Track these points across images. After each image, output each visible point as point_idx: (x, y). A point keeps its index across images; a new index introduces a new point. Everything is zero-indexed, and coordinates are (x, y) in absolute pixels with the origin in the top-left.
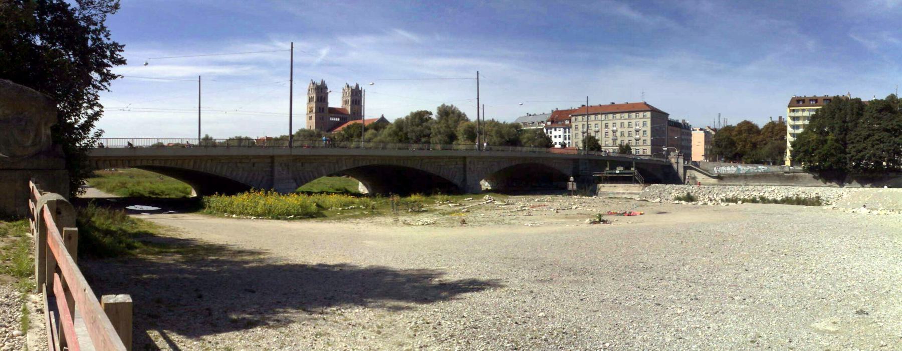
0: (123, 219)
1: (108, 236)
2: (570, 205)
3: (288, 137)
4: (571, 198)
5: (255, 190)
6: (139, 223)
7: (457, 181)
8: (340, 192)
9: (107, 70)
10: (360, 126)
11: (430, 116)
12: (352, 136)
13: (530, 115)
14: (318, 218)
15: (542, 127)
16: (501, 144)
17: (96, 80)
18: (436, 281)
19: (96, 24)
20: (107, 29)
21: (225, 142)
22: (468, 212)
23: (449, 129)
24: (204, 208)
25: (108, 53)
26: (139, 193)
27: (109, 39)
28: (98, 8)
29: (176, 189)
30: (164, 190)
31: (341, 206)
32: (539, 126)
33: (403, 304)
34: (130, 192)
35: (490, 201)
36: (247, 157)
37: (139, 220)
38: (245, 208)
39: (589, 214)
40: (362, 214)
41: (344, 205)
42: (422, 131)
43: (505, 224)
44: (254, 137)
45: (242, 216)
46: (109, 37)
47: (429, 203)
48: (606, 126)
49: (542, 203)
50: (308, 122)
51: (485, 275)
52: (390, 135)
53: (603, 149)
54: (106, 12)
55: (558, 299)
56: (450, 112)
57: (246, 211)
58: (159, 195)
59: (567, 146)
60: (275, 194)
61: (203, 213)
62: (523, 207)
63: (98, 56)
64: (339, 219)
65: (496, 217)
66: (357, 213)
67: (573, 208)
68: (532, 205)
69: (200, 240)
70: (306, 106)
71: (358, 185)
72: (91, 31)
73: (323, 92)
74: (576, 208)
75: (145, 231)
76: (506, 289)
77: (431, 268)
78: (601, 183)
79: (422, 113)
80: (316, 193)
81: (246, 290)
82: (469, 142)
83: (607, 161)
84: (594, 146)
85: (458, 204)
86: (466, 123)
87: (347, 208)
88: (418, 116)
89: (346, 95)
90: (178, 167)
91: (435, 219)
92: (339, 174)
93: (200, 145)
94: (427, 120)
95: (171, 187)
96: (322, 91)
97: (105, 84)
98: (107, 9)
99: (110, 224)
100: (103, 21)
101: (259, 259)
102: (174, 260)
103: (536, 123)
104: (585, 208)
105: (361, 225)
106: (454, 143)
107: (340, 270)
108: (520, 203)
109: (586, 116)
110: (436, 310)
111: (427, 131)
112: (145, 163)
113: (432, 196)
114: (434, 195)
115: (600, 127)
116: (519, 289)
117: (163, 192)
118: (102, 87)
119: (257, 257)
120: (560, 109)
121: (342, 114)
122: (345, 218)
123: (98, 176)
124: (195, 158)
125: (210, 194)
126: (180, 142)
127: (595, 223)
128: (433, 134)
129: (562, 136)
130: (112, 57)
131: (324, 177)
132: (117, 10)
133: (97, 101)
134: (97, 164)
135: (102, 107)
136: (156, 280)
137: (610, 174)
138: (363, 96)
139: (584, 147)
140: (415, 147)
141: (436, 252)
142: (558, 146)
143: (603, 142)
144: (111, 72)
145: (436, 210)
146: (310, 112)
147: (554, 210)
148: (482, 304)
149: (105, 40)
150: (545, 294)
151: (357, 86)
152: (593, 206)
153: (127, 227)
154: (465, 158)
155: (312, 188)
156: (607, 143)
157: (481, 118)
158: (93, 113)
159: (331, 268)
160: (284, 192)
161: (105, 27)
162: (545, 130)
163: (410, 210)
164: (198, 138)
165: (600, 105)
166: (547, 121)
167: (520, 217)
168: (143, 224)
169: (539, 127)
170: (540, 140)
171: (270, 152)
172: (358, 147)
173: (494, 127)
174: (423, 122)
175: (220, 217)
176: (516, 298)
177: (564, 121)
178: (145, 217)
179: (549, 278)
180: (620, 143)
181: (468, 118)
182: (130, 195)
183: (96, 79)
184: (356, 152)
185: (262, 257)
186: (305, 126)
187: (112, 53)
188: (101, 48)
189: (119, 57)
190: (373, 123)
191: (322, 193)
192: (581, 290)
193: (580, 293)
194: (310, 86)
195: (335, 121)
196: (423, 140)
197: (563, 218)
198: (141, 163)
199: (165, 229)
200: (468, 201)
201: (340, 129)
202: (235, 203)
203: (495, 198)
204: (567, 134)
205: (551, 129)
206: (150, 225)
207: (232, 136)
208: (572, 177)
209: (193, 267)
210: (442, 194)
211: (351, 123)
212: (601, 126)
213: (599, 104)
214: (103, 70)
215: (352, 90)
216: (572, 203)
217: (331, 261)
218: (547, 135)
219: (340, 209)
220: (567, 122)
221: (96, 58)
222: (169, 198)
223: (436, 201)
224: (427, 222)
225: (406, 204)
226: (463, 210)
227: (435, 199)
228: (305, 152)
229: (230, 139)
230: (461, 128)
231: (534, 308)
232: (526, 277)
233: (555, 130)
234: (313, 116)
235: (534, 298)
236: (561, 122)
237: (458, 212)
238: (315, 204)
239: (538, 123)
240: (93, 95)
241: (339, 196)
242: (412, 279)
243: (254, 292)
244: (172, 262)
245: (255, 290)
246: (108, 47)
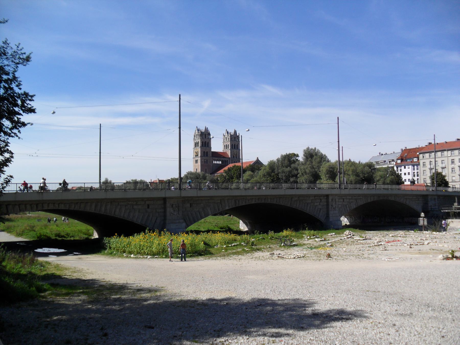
0: (32, 262)
1: (19, 281)
2: (422, 241)
3: (177, 179)
4: (422, 233)
5: (150, 230)
6: (47, 266)
7: (321, 216)
8: (224, 230)
9: (17, 118)
10: (239, 168)
11: (297, 158)
12: (232, 178)
13: (382, 155)
14: (206, 256)
15: (392, 166)
16: (356, 183)
17: (7, 127)
18: (309, 311)
19: (7, 74)
20: (19, 80)
21: (122, 185)
22: (332, 246)
23: (313, 170)
24: (105, 249)
25: (19, 102)
26: (46, 236)
27: (20, 89)
28: (11, 59)
29: (80, 231)
30: (69, 232)
31: (225, 244)
32: (390, 164)
33: (282, 331)
34: (38, 235)
35: (350, 236)
36: (142, 199)
37: (47, 262)
38: (141, 248)
39: (441, 250)
40: (244, 250)
41: (228, 243)
42: (290, 172)
43: (365, 258)
44: (148, 181)
45: (139, 256)
46: (20, 87)
47: (298, 237)
48: (453, 162)
49: (396, 238)
50: (194, 166)
51: (351, 306)
52: (264, 176)
53: (450, 185)
54: (18, 63)
55: (419, 333)
56: (314, 154)
57: (142, 251)
58: (65, 237)
59: (416, 183)
60: (168, 234)
61: (104, 254)
62: (379, 242)
63: (10, 104)
64: (224, 256)
65: (356, 252)
66: (239, 250)
67: (425, 243)
68: (387, 240)
69: (103, 280)
70: (193, 150)
71: (239, 222)
72: (3, 80)
73: (207, 137)
74: (428, 243)
75: (53, 274)
76: (371, 321)
77: (304, 299)
78: (449, 219)
79: (291, 155)
80: (203, 232)
81: (145, 326)
82: (331, 182)
83: (455, 196)
84: (441, 182)
85: (323, 239)
86: (327, 164)
87: (230, 245)
88: (287, 159)
89: (226, 140)
90: (80, 210)
91: (305, 252)
92: (222, 214)
93: (101, 188)
94: (294, 162)
95: (76, 229)
96: (205, 137)
97: (15, 131)
98: (19, 61)
99: (20, 268)
100: (15, 71)
101: (156, 296)
102: (80, 300)
103: (387, 161)
104: (436, 244)
105: (242, 261)
106: (317, 182)
107: (227, 304)
108: (376, 238)
109: (433, 154)
110: (312, 338)
111: (296, 172)
112: (51, 207)
113: (301, 232)
114: (303, 230)
116: (383, 322)
117: (68, 234)
118: (13, 135)
119: (153, 294)
121: (224, 157)
122: (228, 255)
123: (8, 220)
124: (99, 201)
125: (110, 235)
126: (83, 185)
127: (449, 259)
128: (300, 174)
129: (411, 173)
130: (23, 106)
131: (210, 216)
132: (28, 63)
133: (8, 147)
134: (7, 209)
135: (12, 154)
136: (65, 321)
137: (458, 209)
138: (240, 141)
139: (433, 183)
140: (284, 185)
141: (307, 284)
142: (407, 183)
143: (450, 178)
144: (21, 120)
145: (304, 244)
146: (196, 156)
147: (408, 245)
148: (351, 334)
149: (16, 90)
150: (407, 328)
151: (235, 132)
152: (445, 242)
153: (36, 270)
154: (327, 196)
155: (199, 227)
156: (454, 178)
157: (341, 160)
158: (3, 159)
159: (219, 302)
160: (175, 232)
161: (17, 78)
162: (395, 168)
163: (282, 244)
164: (99, 182)
165: (446, 142)
166: (397, 159)
167: (377, 251)
168: (51, 267)
169: (390, 166)
170: (391, 177)
171: (161, 194)
172: (238, 188)
173: (351, 166)
174: (292, 164)
175: (119, 257)
176: (381, 330)
177: (413, 159)
178: (52, 259)
179: (409, 312)
180: (410, 182)
181: (328, 159)
182: (38, 237)
183: (7, 126)
184: (237, 193)
185: (158, 294)
186: (192, 170)
187: (23, 102)
188: (13, 97)
189: (29, 106)
190: (250, 166)
191: (208, 231)
192: (441, 327)
193: (441, 330)
194: (195, 133)
195: (218, 164)
196: (292, 180)
197: (416, 254)
198: (48, 207)
199: (71, 270)
200: (332, 236)
201: (222, 171)
202: (133, 243)
203: (354, 233)
204: (416, 171)
205: (401, 166)
206: (57, 267)
207: (129, 179)
208: (423, 213)
209: (99, 307)
210: (309, 229)
211: (231, 165)
212: (447, 162)
213: (445, 141)
214: (14, 118)
215: (231, 136)
216: (424, 239)
217: (219, 296)
218: (397, 173)
219: (225, 246)
220: (415, 160)
221: (8, 106)
222: (74, 240)
223: (304, 235)
224: (298, 256)
225: (280, 239)
226: (328, 245)
227: (303, 234)
228: (193, 193)
229: (127, 183)
230: (324, 169)
231: (398, 341)
232: (388, 311)
233: (405, 168)
234: (199, 159)
235: (397, 331)
236: (410, 159)
237: (324, 246)
238: (203, 242)
239: (389, 162)
240: (4, 141)
241: (223, 234)
242: (289, 309)
243: (153, 328)
244: (79, 302)
245: (154, 325)
246: (19, 96)
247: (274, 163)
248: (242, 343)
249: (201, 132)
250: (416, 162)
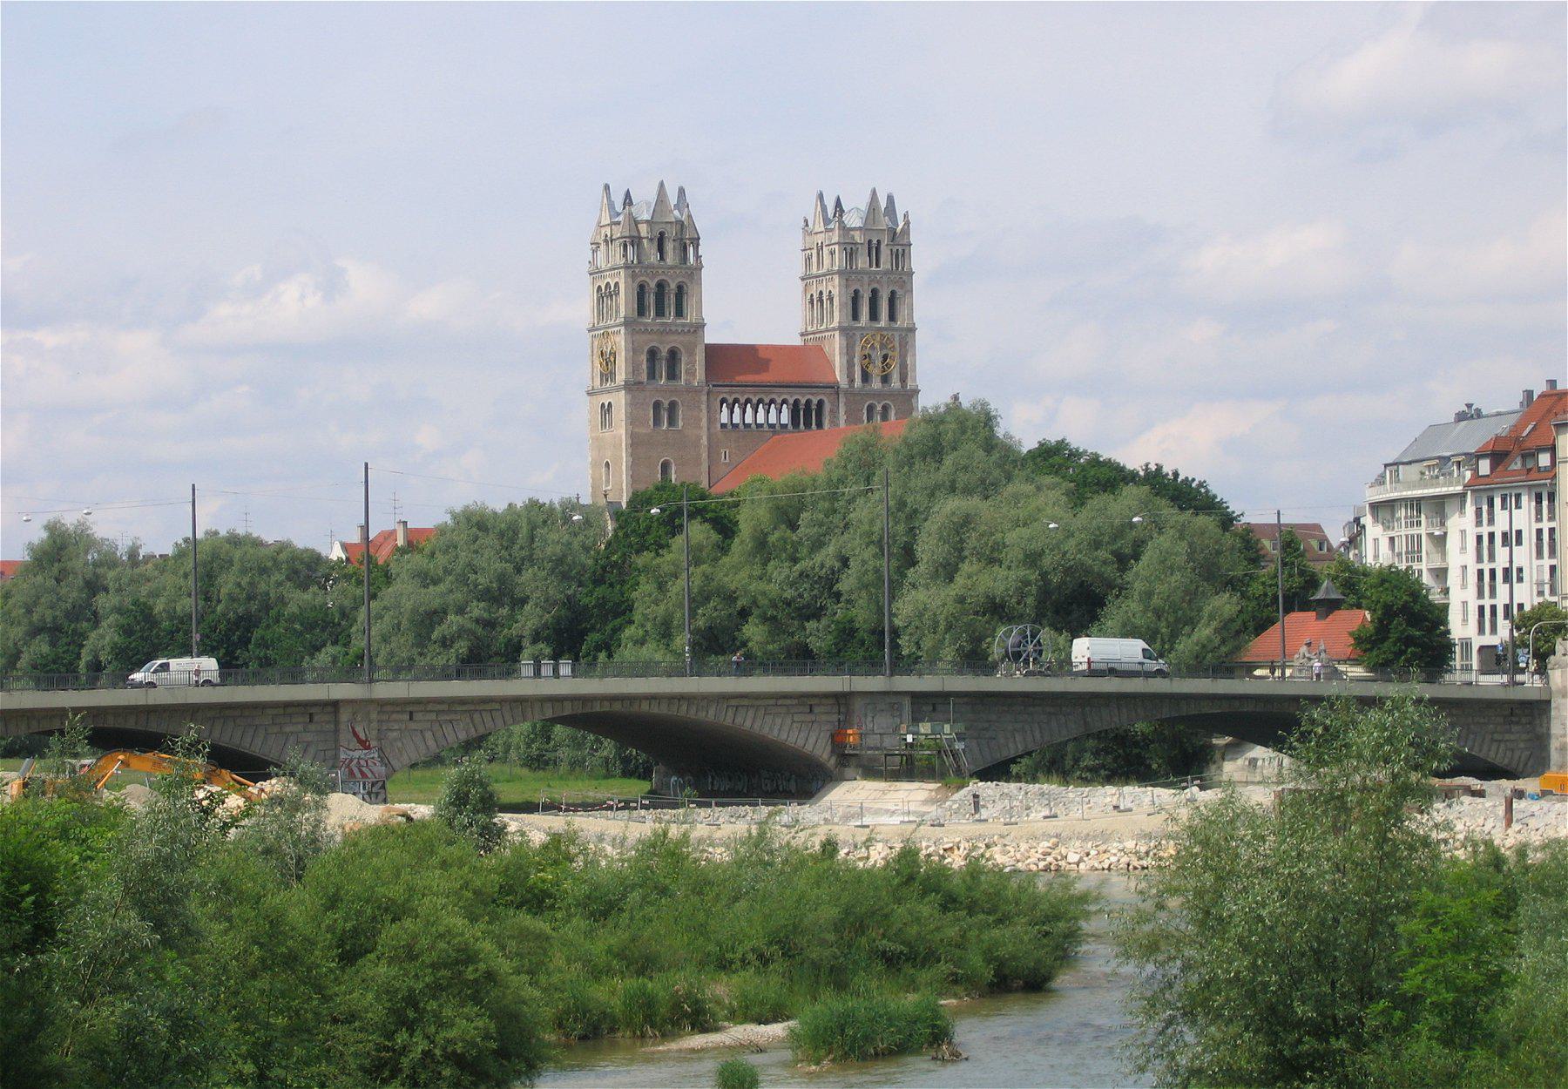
15: (1459, 489)
220: (1544, 460)
234: (620, 400)
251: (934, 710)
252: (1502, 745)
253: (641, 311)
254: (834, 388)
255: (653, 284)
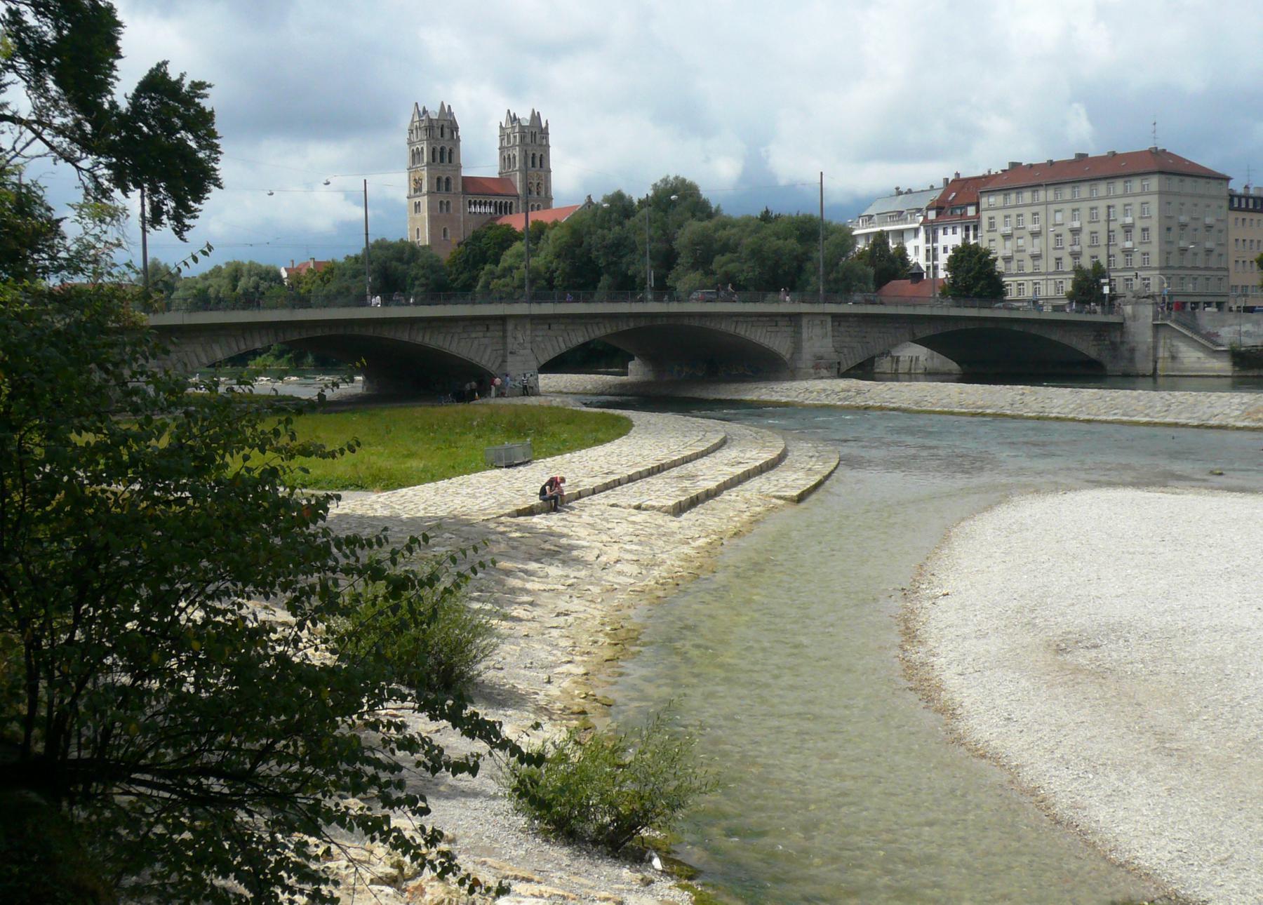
15: (916, 225)
115: (1042, 221)
120: (965, 174)
146: (416, 191)
166: (929, 209)
194: (413, 122)
220: (971, 211)
234: (424, 201)
247: (243, 264)
248: (1084, 882)
249: (431, 120)
250: (972, 217)
251: (488, 328)
252: (476, 342)
253: (434, 160)
254: (517, 196)
255: (439, 148)
